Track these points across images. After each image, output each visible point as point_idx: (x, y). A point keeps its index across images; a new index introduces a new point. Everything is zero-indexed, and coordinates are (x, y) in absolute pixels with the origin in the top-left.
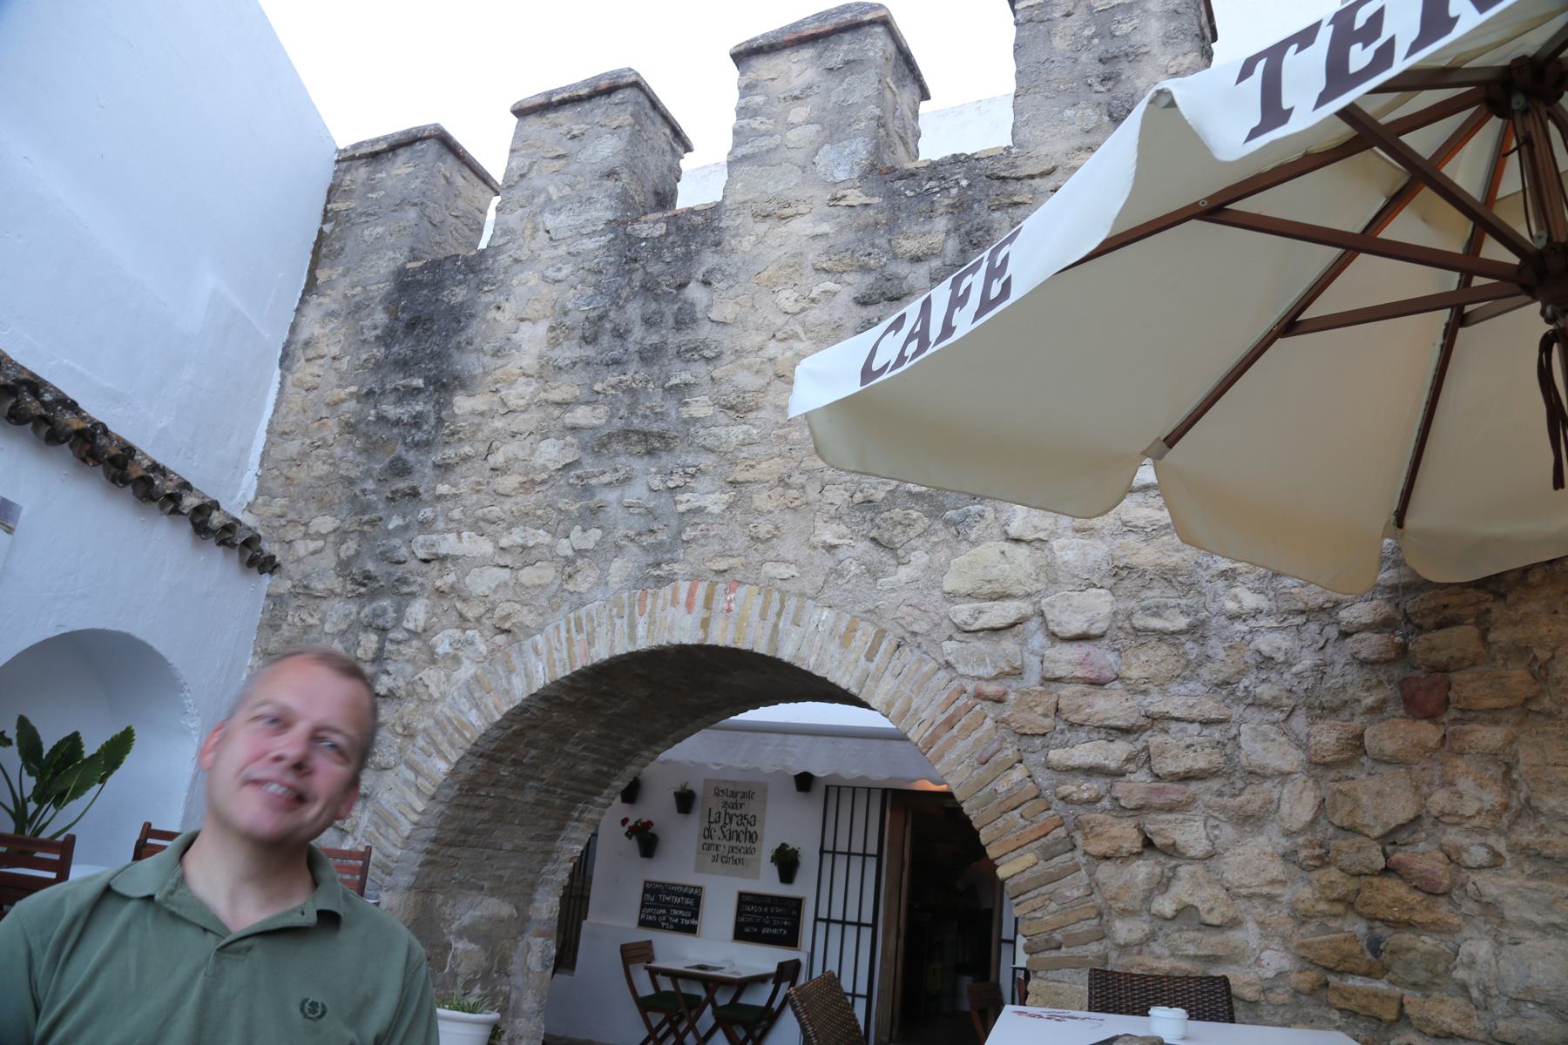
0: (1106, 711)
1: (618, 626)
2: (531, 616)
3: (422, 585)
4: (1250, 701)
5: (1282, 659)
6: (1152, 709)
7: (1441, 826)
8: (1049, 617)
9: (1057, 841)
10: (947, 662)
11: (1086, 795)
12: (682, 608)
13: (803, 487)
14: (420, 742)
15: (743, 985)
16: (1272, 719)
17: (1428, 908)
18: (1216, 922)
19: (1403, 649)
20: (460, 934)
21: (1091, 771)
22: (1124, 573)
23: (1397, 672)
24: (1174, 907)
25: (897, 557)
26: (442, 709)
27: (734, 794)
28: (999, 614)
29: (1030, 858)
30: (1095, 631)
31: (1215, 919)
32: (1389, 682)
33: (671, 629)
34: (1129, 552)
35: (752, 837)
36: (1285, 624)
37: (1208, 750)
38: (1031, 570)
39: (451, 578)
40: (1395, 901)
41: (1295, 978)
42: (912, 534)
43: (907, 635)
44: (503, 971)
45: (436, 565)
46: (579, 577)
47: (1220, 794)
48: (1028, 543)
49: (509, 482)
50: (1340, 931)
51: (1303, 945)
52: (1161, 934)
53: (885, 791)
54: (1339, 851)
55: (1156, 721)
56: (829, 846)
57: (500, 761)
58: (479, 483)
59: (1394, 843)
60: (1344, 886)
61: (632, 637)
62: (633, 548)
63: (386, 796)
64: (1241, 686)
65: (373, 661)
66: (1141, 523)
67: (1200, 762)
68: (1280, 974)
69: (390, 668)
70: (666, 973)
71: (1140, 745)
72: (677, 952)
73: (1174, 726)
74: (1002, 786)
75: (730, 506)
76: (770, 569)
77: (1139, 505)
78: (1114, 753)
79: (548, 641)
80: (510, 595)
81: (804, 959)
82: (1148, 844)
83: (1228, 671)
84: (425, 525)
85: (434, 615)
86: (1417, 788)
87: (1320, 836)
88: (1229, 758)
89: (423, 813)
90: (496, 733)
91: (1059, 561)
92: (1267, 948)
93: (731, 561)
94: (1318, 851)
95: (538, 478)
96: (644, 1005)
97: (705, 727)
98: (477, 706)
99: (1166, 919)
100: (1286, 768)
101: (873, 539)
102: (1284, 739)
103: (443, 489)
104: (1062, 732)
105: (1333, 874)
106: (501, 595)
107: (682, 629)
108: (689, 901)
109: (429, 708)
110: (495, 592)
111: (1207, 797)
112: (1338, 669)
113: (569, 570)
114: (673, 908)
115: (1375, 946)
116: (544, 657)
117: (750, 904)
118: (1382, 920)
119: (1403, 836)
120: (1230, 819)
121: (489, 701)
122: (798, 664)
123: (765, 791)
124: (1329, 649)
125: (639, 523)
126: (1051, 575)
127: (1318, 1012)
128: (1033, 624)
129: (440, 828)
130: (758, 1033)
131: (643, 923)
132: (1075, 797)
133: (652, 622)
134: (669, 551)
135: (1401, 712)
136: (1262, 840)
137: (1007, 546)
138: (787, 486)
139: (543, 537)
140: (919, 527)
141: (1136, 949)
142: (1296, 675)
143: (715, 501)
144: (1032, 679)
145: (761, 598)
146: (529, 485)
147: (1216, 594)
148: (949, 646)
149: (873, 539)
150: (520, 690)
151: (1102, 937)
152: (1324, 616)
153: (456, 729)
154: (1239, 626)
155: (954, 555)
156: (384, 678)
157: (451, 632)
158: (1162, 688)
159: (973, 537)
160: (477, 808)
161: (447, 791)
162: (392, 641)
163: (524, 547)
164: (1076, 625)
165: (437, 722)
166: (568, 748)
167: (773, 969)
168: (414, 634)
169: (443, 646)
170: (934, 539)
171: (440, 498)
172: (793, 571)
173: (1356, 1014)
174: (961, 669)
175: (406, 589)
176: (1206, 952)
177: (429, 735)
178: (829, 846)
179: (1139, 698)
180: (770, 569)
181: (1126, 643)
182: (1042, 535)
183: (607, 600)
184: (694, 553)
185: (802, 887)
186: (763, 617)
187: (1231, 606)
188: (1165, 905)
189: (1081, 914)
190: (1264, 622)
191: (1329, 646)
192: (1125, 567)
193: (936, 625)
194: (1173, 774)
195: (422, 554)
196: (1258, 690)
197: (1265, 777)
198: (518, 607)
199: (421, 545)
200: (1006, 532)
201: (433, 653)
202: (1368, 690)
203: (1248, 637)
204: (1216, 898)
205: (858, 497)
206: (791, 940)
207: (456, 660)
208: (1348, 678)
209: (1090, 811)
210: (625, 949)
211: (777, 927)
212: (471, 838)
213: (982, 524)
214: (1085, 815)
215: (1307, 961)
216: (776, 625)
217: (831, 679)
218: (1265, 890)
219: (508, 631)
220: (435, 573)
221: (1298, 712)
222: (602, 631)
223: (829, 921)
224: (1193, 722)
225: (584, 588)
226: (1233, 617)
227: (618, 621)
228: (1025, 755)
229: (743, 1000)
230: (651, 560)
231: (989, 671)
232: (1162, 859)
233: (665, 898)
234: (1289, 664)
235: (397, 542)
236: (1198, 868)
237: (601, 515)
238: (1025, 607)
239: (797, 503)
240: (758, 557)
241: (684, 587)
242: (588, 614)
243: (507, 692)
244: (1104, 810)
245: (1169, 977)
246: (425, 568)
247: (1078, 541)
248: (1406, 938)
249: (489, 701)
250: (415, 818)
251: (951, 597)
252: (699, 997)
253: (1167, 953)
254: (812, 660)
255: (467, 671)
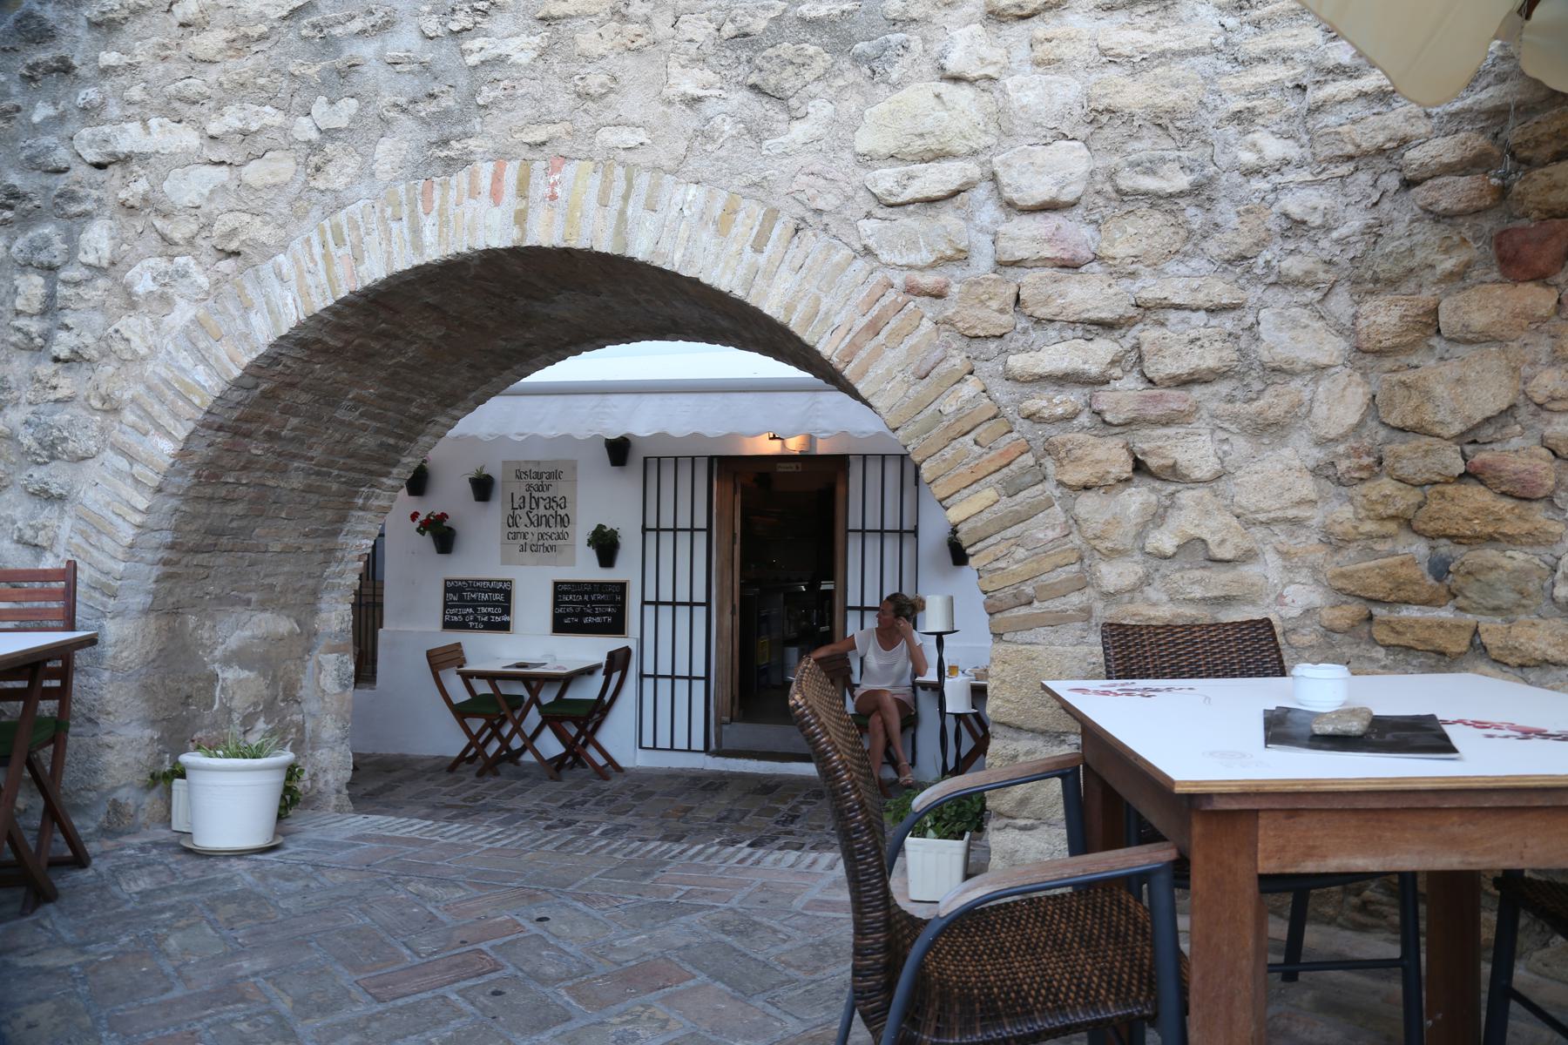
0: (1084, 301)
1: (395, 232)
2: (268, 230)
3: (99, 200)
4: (1272, 279)
5: (1318, 222)
6: (1145, 295)
7: (1545, 415)
8: (1004, 179)
9: (1025, 471)
10: (866, 248)
11: (1060, 411)
12: (485, 200)
13: (647, 20)
14: (129, 416)
15: (567, 680)
16: (1305, 300)
17: (1520, 517)
18: (1228, 556)
19: (1503, 192)
20: (227, 661)
21: (1064, 380)
22: (1104, 119)
23: (1488, 225)
24: (1176, 541)
25: (788, 109)
26: (154, 369)
27: (538, 475)
28: (934, 179)
29: (989, 494)
30: (1066, 197)
31: (1226, 553)
32: (1476, 239)
33: (472, 230)
34: (1111, 90)
35: (564, 521)
36: (1324, 176)
37: (1218, 345)
38: (978, 118)
39: (141, 186)
40: (1477, 511)
41: (1328, 615)
42: (809, 75)
43: (809, 216)
44: (291, 694)
45: (115, 170)
46: (331, 169)
47: (1231, 399)
48: (972, 82)
49: (210, 42)
50: (1393, 554)
51: (1343, 575)
52: (1157, 576)
53: (711, 458)
54: (1398, 457)
55: (1147, 309)
56: (651, 523)
57: (248, 435)
58: (165, 46)
59: (1475, 442)
60: (1405, 499)
61: (417, 245)
62: (406, 122)
63: (91, 494)
64: (1261, 261)
65: (43, 313)
66: (1127, 51)
67: (1208, 359)
68: (1308, 612)
69: (68, 321)
70: (481, 675)
71: (1128, 343)
72: (491, 652)
73: (1173, 316)
74: (949, 406)
75: (543, 54)
76: (608, 136)
77: (1122, 27)
78: (1097, 354)
79: (297, 262)
80: (233, 202)
81: (634, 646)
82: (1139, 467)
83: (1244, 243)
84: (89, 113)
85: (123, 241)
86: (1515, 369)
87: (1367, 442)
88: (1243, 354)
89: (148, 511)
90: (236, 396)
91: (1016, 105)
92: (1292, 582)
93: (552, 129)
94: (1366, 460)
95: (255, 32)
96: (461, 712)
97: (496, 393)
98: (204, 360)
99: (1166, 558)
100: (1323, 360)
101: (754, 87)
102: (1321, 323)
103: (109, 58)
104: (1025, 331)
105: (1387, 486)
106: (219, 204)
107: (492, 229)
108: (498, 597)
109: (135, 370)
110: (210, 200)
111: (1213, 405)
112: (1400, 228)
113: (315, 160)
114: (482, 606)
115: (1440, 569)
116: (293, 283)
117: (567, 593)
118: (1450, 537)
119: (1488, 432)
120: (1243, 430)
121: (221, 351)
122: (658, 263)
123: (575, 468)
124: (1386, 205)
125: (411, 86)
126: (1003, 124)
127: (1356, 651)
128: (982, 192)
129: (176, 529)
130: (590, 728)
131: (447, 625)
132: (1046, 413)
133: (444, 222)
134: (459, 122)
135: (1495, 275)
136: (1287, 452)
137: (945, 88)
138: (624, 18)
139: (271, 116)
140: (818, 67)
141: (1127, 597)
142: (1338, 241)
143: (520, 47)
144: (982, 264)
145: (599, 176)
146: (241, 44)
147: (1227, 143)
148: (867, 226)
149: (754, 87)
150: (263, 332)
151: (1081, 584)
152: (1381, 163)
153: (179, 394)
154: (1258, 184)
155: (868, 104)
156: (62, 336)
157: (152, 262)
158: (1158, 272)
159: (894, 76)
160: (226, 501)
161: (178, 479)
162: (65, 283)
163: (245, 134)
164: (1041, 191)
165: (149, 388)
166: (340, 414)
167: (602, 659)
168: (98, 270)
169: (142, 281)
170: (840, 82)
171: (106, 72)
172: (642, 136)
173: (1408, 648)
174: (885, 256)
175: (74, 208)
176: (1216, 593)
177: (140, 406)
178: (651, 523)
179: (1126, 282)
180: (608, 136)
181: (1106, 212)
182: (991, 71)
183: (376, 198)
184: (497, 123)
185: (625, 570)
186: (603, 204)
187: (1248, 158)
188: (1165, 540)
189: (1058, 560)
190: (1291, 176)
191: (1385, 200)
192: (1107, 110)
193: (848, 198)
194: (1173, 378)
195: (92, 155)
196: (1283, 264)
197: (1293, 374)
198: (246, 218)
199: (88, 142)
200: (942, 68)
201: (130, 295)
202: (1447, 251)
203: (1271, 197)
204: (1228, 526)
205: (729, 29)
206: (616, 626)
207: (165, 300)
208: (1419, 238)
209: (1065, 430)
210: (431, 655)
211: (601, 615)
212: (224, 540)
213: (908, 58)
214: (1058, 435)
215: (1342, 592)
216: (622, 213)
217: (705, 279)
218: (1291, 513)
219: (237, 254)
220: (116, 182)
221: (1338, 289)
222: (373, 241)
223: (657, 603)
224: (1197, 309)
225: (339, 183)
226: (1249, 173)
227: (394, 225)
228: (977, 364)
229: (569, 695)
230: (434, 137)
231: (925, 257)
232: (1157, 484)
233: (468, 595)
234: (1327, 228)
235: (48, 141)
236: (1202, 492)
237: (355, 78)
238: (972, 169)
239: (640, 42)
240: (589, 121)
241: (486, 170)
242: (350, 219)
243: (246, 336)
244: (1083, 428)
245: (1169, 628)
246: (99, 175)
247: (1038, 78)
248: (1490, 554)
249: (221, 351)
250: (138, 519)
251: (866, 160)
252: (521, 697)
253: (1165, 598)
254: (678, 257)
255: (182, 314)
